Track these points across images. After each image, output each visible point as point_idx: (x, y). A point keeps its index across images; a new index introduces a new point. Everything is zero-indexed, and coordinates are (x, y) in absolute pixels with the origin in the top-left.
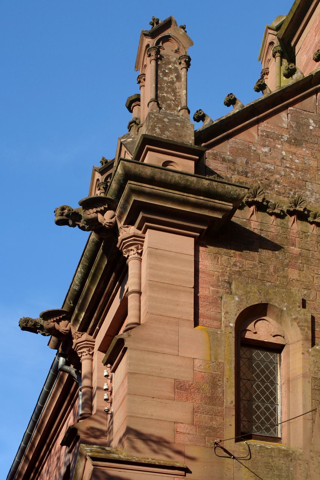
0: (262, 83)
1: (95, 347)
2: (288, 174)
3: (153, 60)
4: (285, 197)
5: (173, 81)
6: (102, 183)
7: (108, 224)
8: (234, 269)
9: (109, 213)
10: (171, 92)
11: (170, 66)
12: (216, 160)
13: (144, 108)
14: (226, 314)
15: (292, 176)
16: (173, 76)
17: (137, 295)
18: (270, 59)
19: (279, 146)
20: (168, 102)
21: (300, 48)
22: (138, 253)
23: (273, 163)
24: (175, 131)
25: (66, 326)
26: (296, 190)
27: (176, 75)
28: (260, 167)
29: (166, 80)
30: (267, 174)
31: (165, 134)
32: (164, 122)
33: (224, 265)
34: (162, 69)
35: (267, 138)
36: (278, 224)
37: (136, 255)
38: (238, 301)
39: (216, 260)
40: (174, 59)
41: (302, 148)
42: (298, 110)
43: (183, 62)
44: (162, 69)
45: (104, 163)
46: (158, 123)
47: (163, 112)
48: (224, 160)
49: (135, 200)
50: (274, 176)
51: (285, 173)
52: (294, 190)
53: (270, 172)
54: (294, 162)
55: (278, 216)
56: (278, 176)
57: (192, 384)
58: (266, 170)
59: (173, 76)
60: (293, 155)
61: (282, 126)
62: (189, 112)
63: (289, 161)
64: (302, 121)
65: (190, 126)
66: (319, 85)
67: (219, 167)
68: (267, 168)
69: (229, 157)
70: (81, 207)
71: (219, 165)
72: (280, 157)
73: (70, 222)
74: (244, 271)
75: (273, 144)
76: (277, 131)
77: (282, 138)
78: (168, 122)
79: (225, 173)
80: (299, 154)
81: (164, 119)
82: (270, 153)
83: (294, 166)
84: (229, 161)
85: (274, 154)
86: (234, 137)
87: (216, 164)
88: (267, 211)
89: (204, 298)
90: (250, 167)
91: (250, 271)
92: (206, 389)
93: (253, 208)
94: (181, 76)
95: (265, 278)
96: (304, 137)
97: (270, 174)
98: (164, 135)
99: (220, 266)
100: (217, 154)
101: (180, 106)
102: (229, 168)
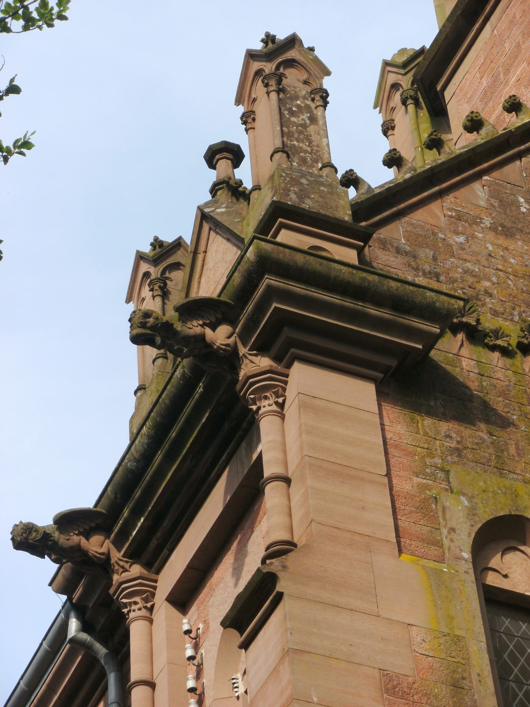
0: (436, 137)
1: (158, 592)
2: (502, 281)
3: (273, 91)
4: (505, 319)
5: (306, 124)
6: (158, 279)
7: (224, 347)
8: (448, 444)
9: (224, 330)
10: (305, 140)
11: (299, 102)
12: (386, 250)
13: (257, 161)
14: (451, 531)
15: (511, 285)
16: (304, 117)
17: (283, 484)
18: (395, 108)
19: (480, 235)
20: (302, 154)
21: (454, 94)
22: (276, 403)
23: (475, 262)
24: (320, 200)
25: (100, 544)
26: (520, 309)
27: (308, 115)
28: (457, 267)
29: (294, 122)
30: (471, 280)
31: (305, 203)
32: (301, 184)
33: (430, 435)
34: (287, 105)
35: (459, 221)
36: (507, 366)
37: (274, 408)
38: (469, 508)
39: (415, 425)
40: (304, 92)
41: (516, 241)
42: (497, 181)
43: (317, 98)
44: (287, 105)
45: (157, 246)
46: (293, 185)
47: (296, 169)
48: (398, 251)
49: (275, 307)
50: (482, 282)
51: (498, 280)
52: (518, 309)
53: (473, 276)
54: (509, 262)
55: (506, 352)
56: (487, 284)
57: (414, 683)
58: (466, 271)
59: (305, 116)
60: (505, 251)
61: (478, 204)
62: (336, 171)
63: (501, 260)
64: (507, 199)
65: (342, 193)
66: (527, 145)
67: (393, 261)
68: (469, 269)
69: (405, 246)
70: (177, 314)
71: (391, 259)
72: (485, 252)
73: (158, 340)
74: (466, 449)
75: (469, 231)
76: (472, 211)
77: (481, 222)
78: (308, 185)
79: (404, 273)
80: (514, 250)
81: (301, 180)
82: (468, 244)
83: (510, 269)
84: (407, 253)
85: (474, 248)
86: (408, 216)
87: (387, 257)
88: (486, 341)
89: (405, 498)
90: (441, 266)
91: (476, 450)
92: (443, 695)
93: (461, 336)
94: (317, 118)
95: (504, 465)
96: (515, 223)
97: (475, 280)
98: (304, 205)
99: (424, 438)
100: (386, 241)
101: (320, 161)
102: (408, 264)
